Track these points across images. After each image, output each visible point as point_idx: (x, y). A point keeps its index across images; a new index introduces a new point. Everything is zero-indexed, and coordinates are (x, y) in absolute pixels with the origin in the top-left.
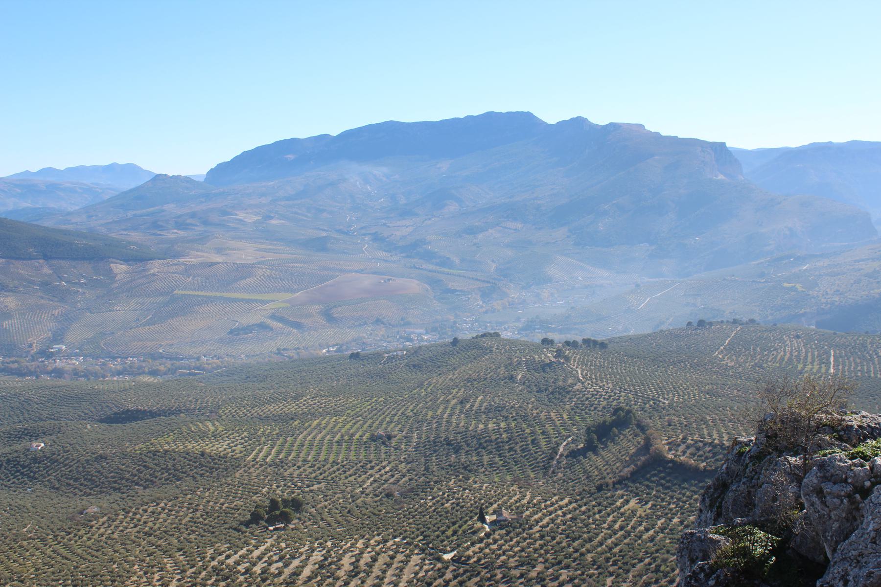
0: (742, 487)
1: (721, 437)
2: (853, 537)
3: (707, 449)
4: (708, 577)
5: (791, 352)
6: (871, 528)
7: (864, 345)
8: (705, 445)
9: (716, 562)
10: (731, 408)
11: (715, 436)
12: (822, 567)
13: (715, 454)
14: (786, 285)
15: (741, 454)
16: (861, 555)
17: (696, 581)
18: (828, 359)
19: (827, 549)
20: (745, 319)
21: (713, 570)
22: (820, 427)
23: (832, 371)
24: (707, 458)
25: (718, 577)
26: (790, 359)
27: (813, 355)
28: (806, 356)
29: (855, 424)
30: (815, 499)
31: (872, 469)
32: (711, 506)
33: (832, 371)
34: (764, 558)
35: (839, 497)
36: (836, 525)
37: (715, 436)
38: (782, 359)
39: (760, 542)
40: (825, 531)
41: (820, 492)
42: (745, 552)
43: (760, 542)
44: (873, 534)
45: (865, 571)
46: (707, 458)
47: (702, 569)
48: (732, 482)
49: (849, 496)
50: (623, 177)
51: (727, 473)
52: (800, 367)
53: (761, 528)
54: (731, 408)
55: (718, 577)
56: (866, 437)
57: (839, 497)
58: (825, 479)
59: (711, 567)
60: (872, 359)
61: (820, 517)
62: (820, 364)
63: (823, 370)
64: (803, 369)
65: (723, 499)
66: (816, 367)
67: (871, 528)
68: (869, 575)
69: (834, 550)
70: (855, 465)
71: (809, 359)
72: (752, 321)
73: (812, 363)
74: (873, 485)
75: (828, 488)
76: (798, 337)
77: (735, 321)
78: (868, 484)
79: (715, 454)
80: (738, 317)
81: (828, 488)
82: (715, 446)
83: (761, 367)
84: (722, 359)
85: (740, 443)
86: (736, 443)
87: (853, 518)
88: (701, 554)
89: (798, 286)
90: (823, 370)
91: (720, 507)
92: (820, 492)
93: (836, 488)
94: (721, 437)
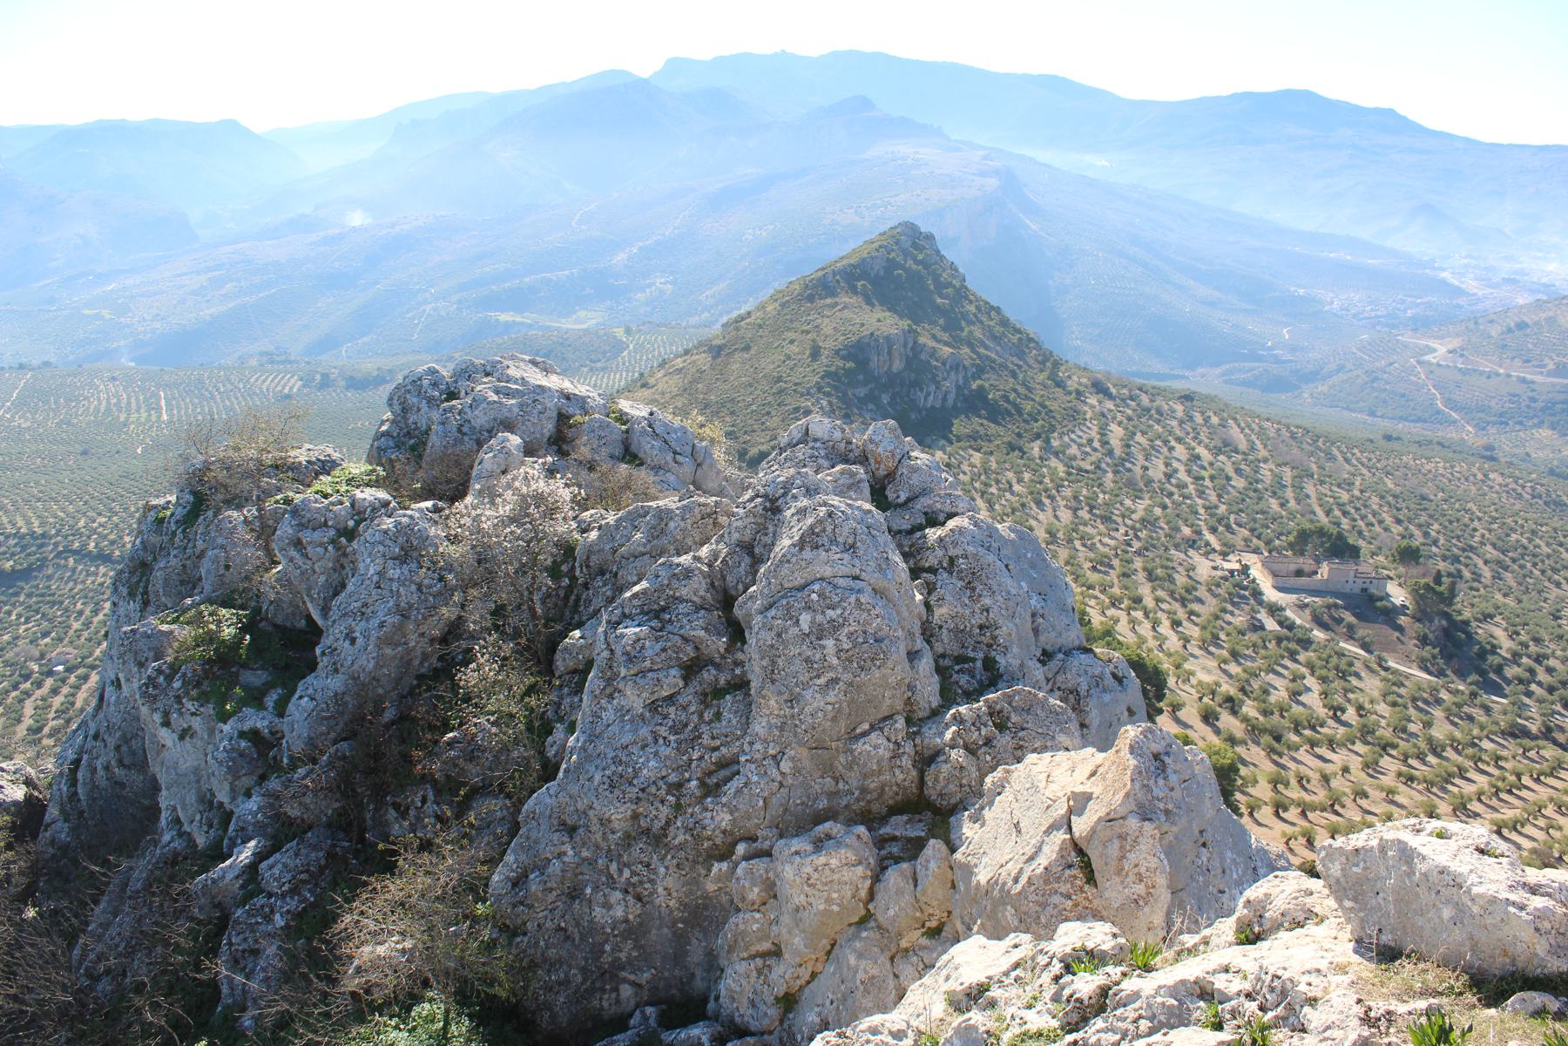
0: (174, 562)
1: (29, 523)
2: (350, 587)
3: (12, 542)
4: (170, 678)
5: (108, 402)
6: (372, 571)
7: (200, 381)
8: (7, 537)
9: (176, 659)
10: (37, 483)
11: (20, 523)
12: (314, 633)
13: (24, 548)
14: (87, 312)
15: (160, 521)
16: (365, 605)
17: (155, 687)
18: (158, 404)
19: (311, 610)
20: (35, 363)
21: (174, 669)
22: (261, 469)
23: (165, 417)
24: (13, 554)
25: (184, 675)
26: (108, 410)
27: (137, 399)
28: (129, 403)
29: (303, 459)
30: (293, 553)
31: (353, 505)
32: (132, 595)
33: (165, 417)
34: (238, 640)
35: (321, 545)
36: (322, 579)
37: (20, 523)
38: (97, 410)
39: (227, 624)
40: (309, 589)
41: (298, 544)
42: (211, 638)
43: (227, 624)
44: (375, 578)
45: (375, 622)
46: (13, 554)
47: (159, 671)
48: (155, 559)
49: (333, 541)
50: (706, 100)
51: (145, 548)
52: (122, 418)
53: (225, 605)
54: (37, 483)
55: (184, 675)
56: (317, 474)
57: (321, 545)
58: (302, 526)
59: (171, 666)
60: (213, 397)
61: (302, 573)
62: (148, 411)
63: (154, 418)
64: (127, 419)
65: (148, 581)
66: (144, 415)
67: (372, 571)
68: (382, 625)
69: (325, 610)
70: (333, 504)
71: (134, 406)
72: (47, 364)
73: (138, 411)
74: (358, 523)
75: (307, 536)
76: (114, 379)
77: (21, 367)
78: (351, 523)
79: (24, 548)
80: (24, 360)
81: (307, 536)
82: (23, 537)
83: (69, 423)
84: (12, 419)
85: (155, 507)
86: (148, 508)
87: (343, 566)
88: (152, 654)
89: (106, 313)
90: (154, 418)
91: (146, 592)
92: (298, 544)
93: (317, 536)
94: (29, 523)
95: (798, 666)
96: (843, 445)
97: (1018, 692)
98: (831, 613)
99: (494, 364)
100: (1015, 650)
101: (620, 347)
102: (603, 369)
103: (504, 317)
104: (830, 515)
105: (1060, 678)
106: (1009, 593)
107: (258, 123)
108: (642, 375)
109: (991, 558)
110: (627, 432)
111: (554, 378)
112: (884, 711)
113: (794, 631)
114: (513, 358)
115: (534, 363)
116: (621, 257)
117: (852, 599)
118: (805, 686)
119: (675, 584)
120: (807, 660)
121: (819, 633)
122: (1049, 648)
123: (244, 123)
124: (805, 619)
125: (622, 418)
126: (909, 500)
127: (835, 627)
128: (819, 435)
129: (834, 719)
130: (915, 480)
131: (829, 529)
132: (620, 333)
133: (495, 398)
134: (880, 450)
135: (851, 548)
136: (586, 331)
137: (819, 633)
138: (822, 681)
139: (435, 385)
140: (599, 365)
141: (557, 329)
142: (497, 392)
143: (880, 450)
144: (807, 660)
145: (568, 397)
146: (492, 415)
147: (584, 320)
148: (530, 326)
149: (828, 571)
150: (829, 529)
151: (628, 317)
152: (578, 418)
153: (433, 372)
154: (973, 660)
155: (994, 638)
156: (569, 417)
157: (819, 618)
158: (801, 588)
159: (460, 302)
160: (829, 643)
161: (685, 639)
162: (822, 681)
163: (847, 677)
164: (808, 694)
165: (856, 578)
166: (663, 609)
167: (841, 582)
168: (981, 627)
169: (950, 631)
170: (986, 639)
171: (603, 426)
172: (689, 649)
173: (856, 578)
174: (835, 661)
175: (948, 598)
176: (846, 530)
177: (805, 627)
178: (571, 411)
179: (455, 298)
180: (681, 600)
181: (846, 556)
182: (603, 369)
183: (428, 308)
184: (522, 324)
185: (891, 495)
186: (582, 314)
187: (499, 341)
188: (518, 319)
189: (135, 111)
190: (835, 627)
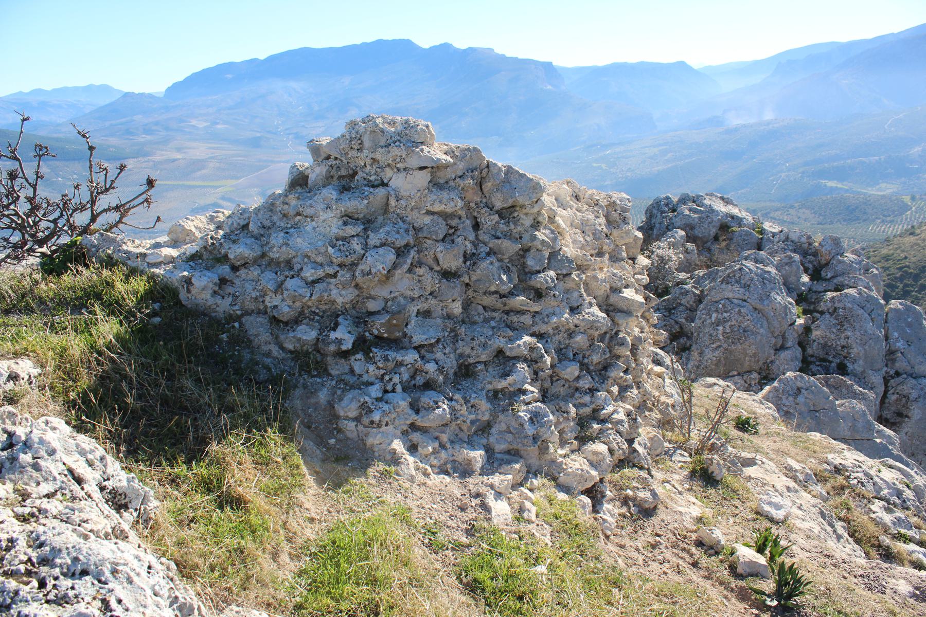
89: (603, 166)
95: (707, 338)
96: (806, 246)
97: (834, 378)
98: (725, 314)
99: (698, 196)
100: (861, 362)
101: (905, 208)
102: (891, 221)
103: (831, 184)
104: (740, 269)
105: (900, 388)
106: (866, 332)
107: (696, 62)
108: (913, 227)
109: (861, 311)
110: (761, 239)
111: (730, 207)
112: (746, 366)
113: (709, 321)
114: (712, 195)
115: (722, 198)
116: (917, 150)
117: (737, 310)
118: (707, 347)
119: (681, 297)
120: (711, 335)
121: (718, 323)
122: (901, 371)
123: (689, 63)
124: (714, 315)
125: (762, 232)
126: (833, 277)
127: (725, 321)
128: (794, 238)
129: (716, 365)
130: (840, 268)
131: (738, 275)
132: (907, 199)
133: (687, 212)
134: (823, 250)
135: (747, 287)
136: (884, 196)
137: (718, 323)
138: (714, 346)
139: (667, 205)
140: (888, 219)
141: (865, 194)
142: (690, 210)
143: (823, 250)
144: (711, 335)
145: (733, 217)
146: (684, 221)
147: (886, 189)
148: (847, 191)
149: (731, 295)
150: (738, 275)
151: (915, 189)
152: (734, 229)
153: (667, 198)
154: (831, 362)
155: (849, 353)
156: (729, 227)
157: (720, 316)
158: (716, 302)
159: (803, 173)
160: (721, 328)
161: (676, 322)
162: (714, 346)
163: (725, 345)
164: (707, 351)
165: (745, 301)
166: (674, 308)
167: (735, 301)
168: (843, 347)
169: (819, 344)
170: (844, 353)
171: (748, 234)
172: (677, 327)
173: (745, 301)
174: (721, 337)
175: (823, 327)
176: (747, 278)
177: (713, 319)
178: (732, 224)
179: (801, 170)
180: (681, 305)
181: (742, 290)
182: (891, 221)
183: (783, 175)
184: (841, 189)
185: (823, 274)
186: (883, 185)
187: (824, 198)
188: (839, 186)
189: (632, 57)
190: (725, 321)
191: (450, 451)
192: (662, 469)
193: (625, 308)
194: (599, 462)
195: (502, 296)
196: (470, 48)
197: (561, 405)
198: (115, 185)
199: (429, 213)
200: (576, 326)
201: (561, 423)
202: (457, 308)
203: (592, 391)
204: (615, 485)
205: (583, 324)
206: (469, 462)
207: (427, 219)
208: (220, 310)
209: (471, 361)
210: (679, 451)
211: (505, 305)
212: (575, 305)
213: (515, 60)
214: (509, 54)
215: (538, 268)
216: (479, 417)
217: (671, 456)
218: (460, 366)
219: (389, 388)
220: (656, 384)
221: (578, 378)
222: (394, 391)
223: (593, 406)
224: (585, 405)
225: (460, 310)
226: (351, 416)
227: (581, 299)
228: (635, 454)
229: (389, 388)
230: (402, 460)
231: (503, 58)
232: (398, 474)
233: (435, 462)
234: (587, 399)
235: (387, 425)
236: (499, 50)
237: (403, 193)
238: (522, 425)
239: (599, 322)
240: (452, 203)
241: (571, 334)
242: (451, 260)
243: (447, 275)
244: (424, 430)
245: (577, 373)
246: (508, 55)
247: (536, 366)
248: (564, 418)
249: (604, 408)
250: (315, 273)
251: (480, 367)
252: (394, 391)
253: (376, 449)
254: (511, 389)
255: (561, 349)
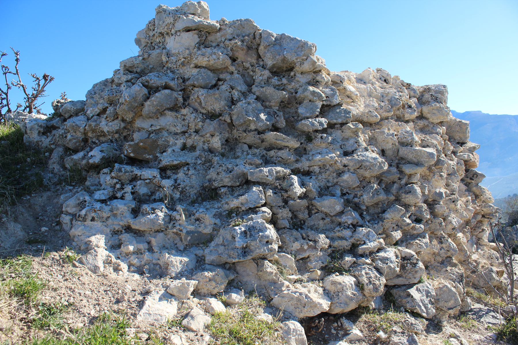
191: (156, 255)
192: (461, 327)
193: (415, 160)
194: (337, 293)
195: (259, 133)
196: (466, 112)
197: (309, 233)
198: (45, 89)
199: (196, 67)
200: (345, 166)
201: (305, 251)
202: (216, 143)
203: (355, 227)
204: (370, 326)
205: (351, 164)
206: (167, 265)
207: (195, 71)
208: (44, 145)
209: (216, 184)
210: (492, 313)
211: (263, 141)
212: (350, 149)
213: (496, 116)
214: (492, 112)
215: (308, 115)
216: (200, 230)
217: (481, 317)
218: (204, 188)
219: (119, 195)
220: (487, 255)
221: (342, 213)
222: (122, 198)
223: (352, 240)
224: (342, 238)
225: (219, 144)
226: (70, 211)
227: (356, 145)
228: (409, 299)
229: (119, 195)
230: (93, 251)
231: (488, 115)
232: (81, 262)
233: (135, 261)
234: (347, 233)
235: (93, 219)
236: (485, 111)
237: (173, 51)
238: (234, 238)
239: (367, 161)
240: (218, 58)
241: (340, 174)
242: (214, 103)
243: (212, 116)
244: (138, 234)
245: (338, 208)
246: (491, 114)
247: (285, 195)
248: (310, 247)
249: (365, 243)
250: (93, 110)
251: (223, 190)
252: (122, 198)
253: (76, 239)
254: (243, 208)
255: (328, 187)
